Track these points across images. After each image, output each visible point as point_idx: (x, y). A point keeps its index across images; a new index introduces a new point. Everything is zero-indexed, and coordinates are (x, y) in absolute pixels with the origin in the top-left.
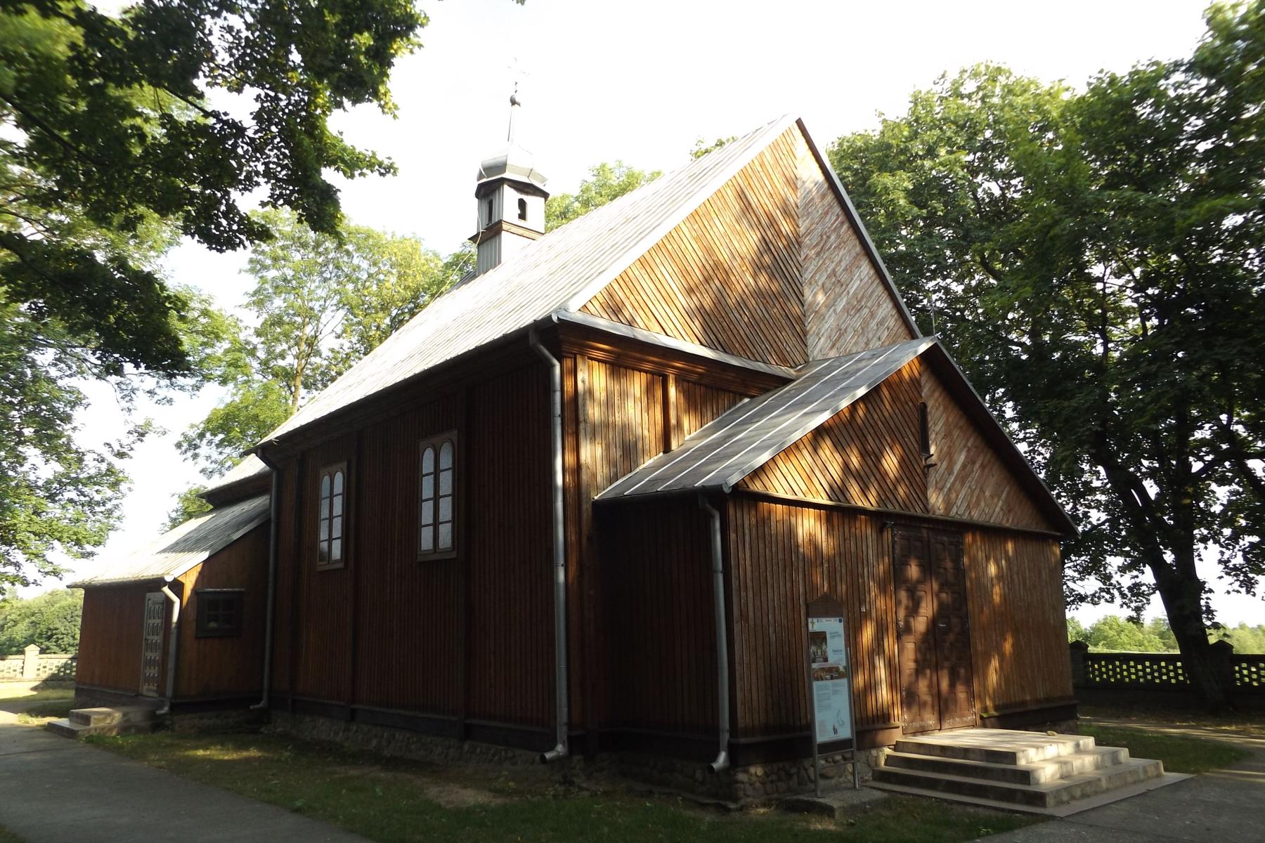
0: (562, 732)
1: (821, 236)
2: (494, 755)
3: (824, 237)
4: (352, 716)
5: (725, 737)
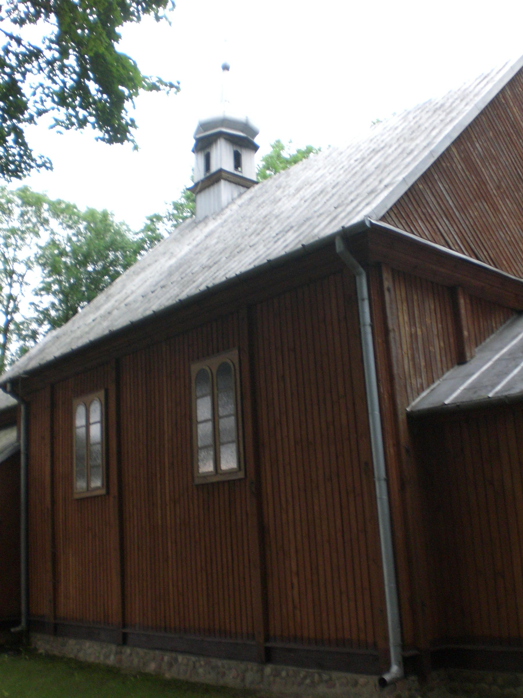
0: (394, 654)
2: (305, 678)
4: (124, 640)
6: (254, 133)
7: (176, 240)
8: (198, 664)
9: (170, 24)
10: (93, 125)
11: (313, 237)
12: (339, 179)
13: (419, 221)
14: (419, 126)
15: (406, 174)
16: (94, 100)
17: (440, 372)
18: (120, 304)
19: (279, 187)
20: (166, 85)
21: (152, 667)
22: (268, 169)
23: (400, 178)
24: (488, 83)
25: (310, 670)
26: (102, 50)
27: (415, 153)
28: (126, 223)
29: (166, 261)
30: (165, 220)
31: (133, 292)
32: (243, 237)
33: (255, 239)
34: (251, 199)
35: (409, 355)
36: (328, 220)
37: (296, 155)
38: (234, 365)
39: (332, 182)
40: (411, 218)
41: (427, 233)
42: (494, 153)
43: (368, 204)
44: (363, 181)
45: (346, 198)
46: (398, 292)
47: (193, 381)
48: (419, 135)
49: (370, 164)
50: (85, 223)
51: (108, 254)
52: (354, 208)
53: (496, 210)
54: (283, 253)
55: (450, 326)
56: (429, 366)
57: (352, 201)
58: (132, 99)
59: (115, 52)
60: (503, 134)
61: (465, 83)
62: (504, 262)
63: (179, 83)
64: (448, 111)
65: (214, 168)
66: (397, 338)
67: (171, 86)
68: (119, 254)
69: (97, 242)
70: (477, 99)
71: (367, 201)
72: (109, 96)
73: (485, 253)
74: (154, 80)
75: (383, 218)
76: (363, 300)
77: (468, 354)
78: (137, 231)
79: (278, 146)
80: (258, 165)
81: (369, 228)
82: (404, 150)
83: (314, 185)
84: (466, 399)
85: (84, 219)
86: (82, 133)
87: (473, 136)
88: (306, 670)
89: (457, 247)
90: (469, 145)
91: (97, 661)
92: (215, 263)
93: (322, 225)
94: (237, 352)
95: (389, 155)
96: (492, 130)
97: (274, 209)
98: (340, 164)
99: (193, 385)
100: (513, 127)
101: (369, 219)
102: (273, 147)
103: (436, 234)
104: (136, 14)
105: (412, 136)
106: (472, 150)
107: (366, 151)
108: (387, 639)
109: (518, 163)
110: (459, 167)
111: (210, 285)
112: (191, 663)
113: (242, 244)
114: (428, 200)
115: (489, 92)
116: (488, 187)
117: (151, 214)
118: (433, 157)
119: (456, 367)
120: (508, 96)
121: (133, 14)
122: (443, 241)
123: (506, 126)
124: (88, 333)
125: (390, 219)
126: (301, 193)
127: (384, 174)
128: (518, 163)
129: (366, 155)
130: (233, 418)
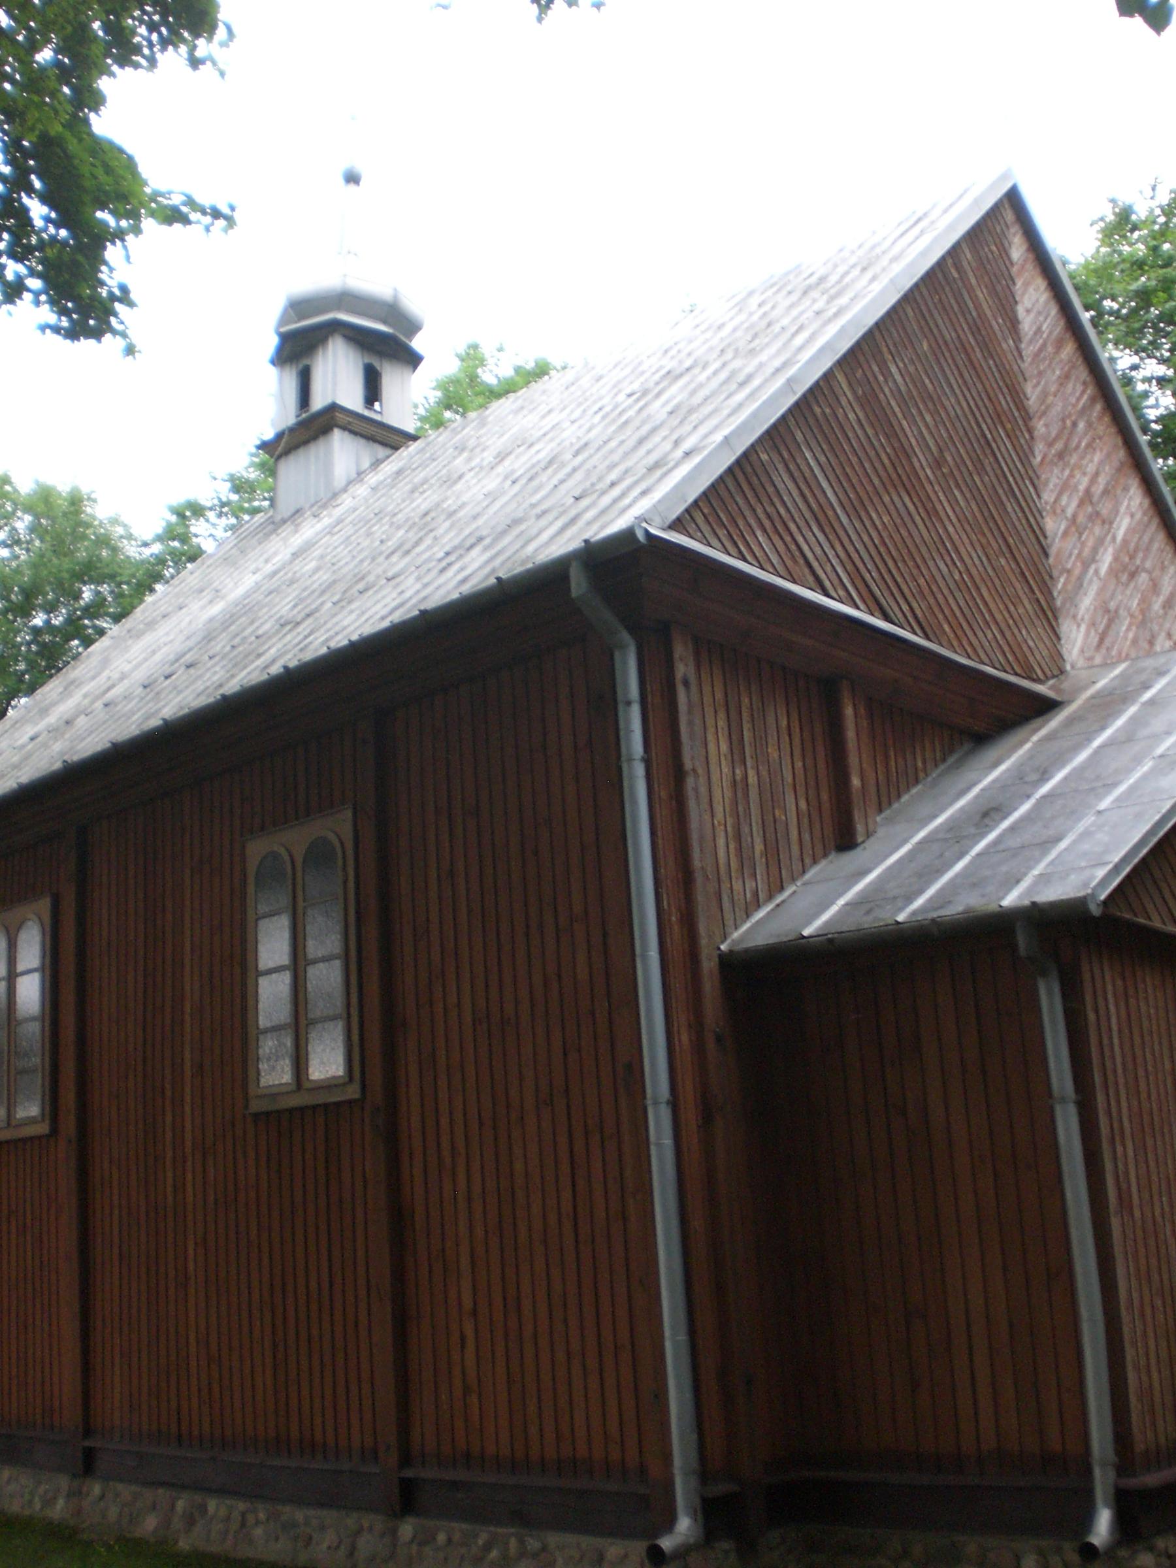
0: (683, 1490)
1: (1063, 420)
2: (487, 1548)
3: (1068, 423)
4: (88, 1465)
5: (1103, 1480)
6: (413, 327)
7: (227, 561)
8: (251, 1518)
9: (222, 74)
10: (37, 294)
11: (524, 562)
12: (592, 435)
13: (759, 533)
14: (769, 325)
15: (733, 427)
16: (41, 240)
17: (797, 866)
18: (93, 702)
19: (460, 449)
20: (204, 213)
21: (150, 1524)
22: (448, 407)
23: (718, 437)
24: (922, 232)
25: (500, 1530)
26: (56, 129)
27: (756, 382)
28: (124, 519)
29: (203, 608)
30: (211, 515)
31: (123, 676)
32: (373, 559)
33: (398, 564)
34: (399, 473)
35: (729, 829)
36: (559, 524)
37: (512, 378)
38: (342, 844)
39: (574, 440)
40: (741, 523)
41: (775, 560)
42: (930, 386)
43: (644, 493)
44: (641, 442)
45: (600, 479)
46: (707, 689)
47: (251, 880)
48: (767, 345)
49: (658, 404)
50: (28, 518)
51: (81, 592)
52: (615, 501)
53: (931, 513)
54: (455, 596)
55: (822, 766)
56: (773, 851)
57: (613, 484)
58: (123, 240)
59: (91, 134)
60: (952, 346)
61: (874, 233)
62: (946, 627)
63: (233, 209)
64: (833, 291)
65: (318, 402)
66: (703, 790)
67: (216, 214)
68: (105, 588)
69: (55, 561)
70: (897, 268)
71: (643, 486)
72: (74, 235)
73: (905, 607)
74: (176, 200)
75: (677, 525)
76: (629, 703)
77: (860, 828)
78: (148, 537)
79: (473, 357)
80: (426, 398)
81: (643, 546)
82: (733, 373)
83: (536, 448)
84: (849, 925)
85: (28, 509)
86: (10, 314)
87: (885, 350)
88: (492, 1529)
89: (842, 593)
90: (875, 368)
91: (27, 1512)
92: (308, 616)
93: (545, 536)
94: (349, 814)
95: (701, 386)
96: (926, 337)
97: (446, 499)
98: (595, 402)
99: (251, 889)
100: (976, 330)
101: (644, 525)
102: (462, 360)
103: (795, 562)
104: (146, 51)
105: (753, 345)
106: (881, 378)
107: (654, 374)
108: (667, 1457)
109: (983, 410)
110: (851, 416)
111: (293, 664)
112: (236, 1515)
113: (369, 572)
114: (781, 486)
115: (923, 254)
116: (915, 460)
117: (179, 499)
118: (794, 393)
119: (833, 856)
120: (965, 264)
121: (137, 50)
122: (811, 579)
123: (958, 328)
124: (16, 767)
125: (694, 526)
126: (507, 463)
127: (687, 427)
128: (983, 410)
129: (651, 384)
130: (337, 964)
